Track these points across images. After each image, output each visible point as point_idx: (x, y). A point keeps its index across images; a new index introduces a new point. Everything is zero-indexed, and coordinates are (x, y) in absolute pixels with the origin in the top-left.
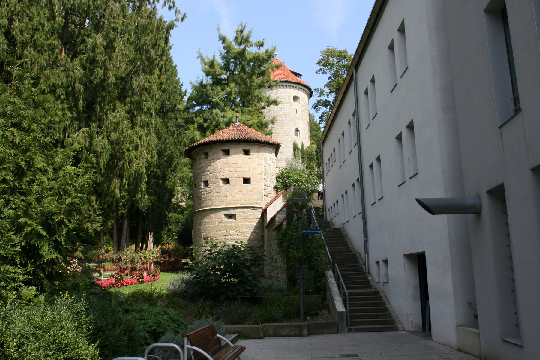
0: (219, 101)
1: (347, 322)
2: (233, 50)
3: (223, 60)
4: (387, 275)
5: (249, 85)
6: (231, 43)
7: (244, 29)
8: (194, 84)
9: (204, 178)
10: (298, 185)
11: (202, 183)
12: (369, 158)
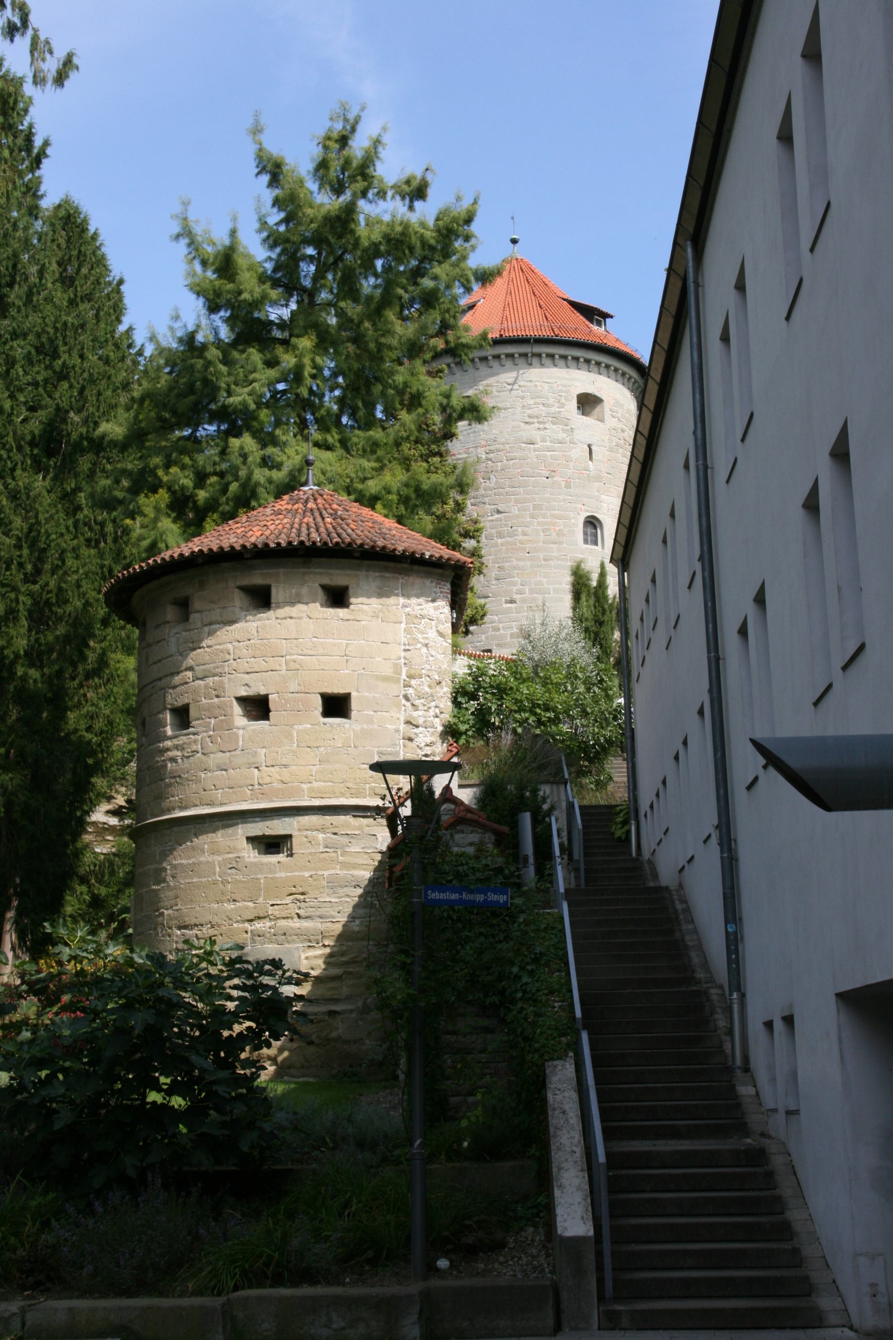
0: (253, 406)
1: (600, 1281)
2: (309, 211)
3: (272, 247)
4: (794, 1076)
5: (372, 346)
6: (301, 181)
7: (353, 130)
8: (164, 344)
9: (174, 698)
10: (540, 723)
11: (168, 716)
12: (735, 605)
